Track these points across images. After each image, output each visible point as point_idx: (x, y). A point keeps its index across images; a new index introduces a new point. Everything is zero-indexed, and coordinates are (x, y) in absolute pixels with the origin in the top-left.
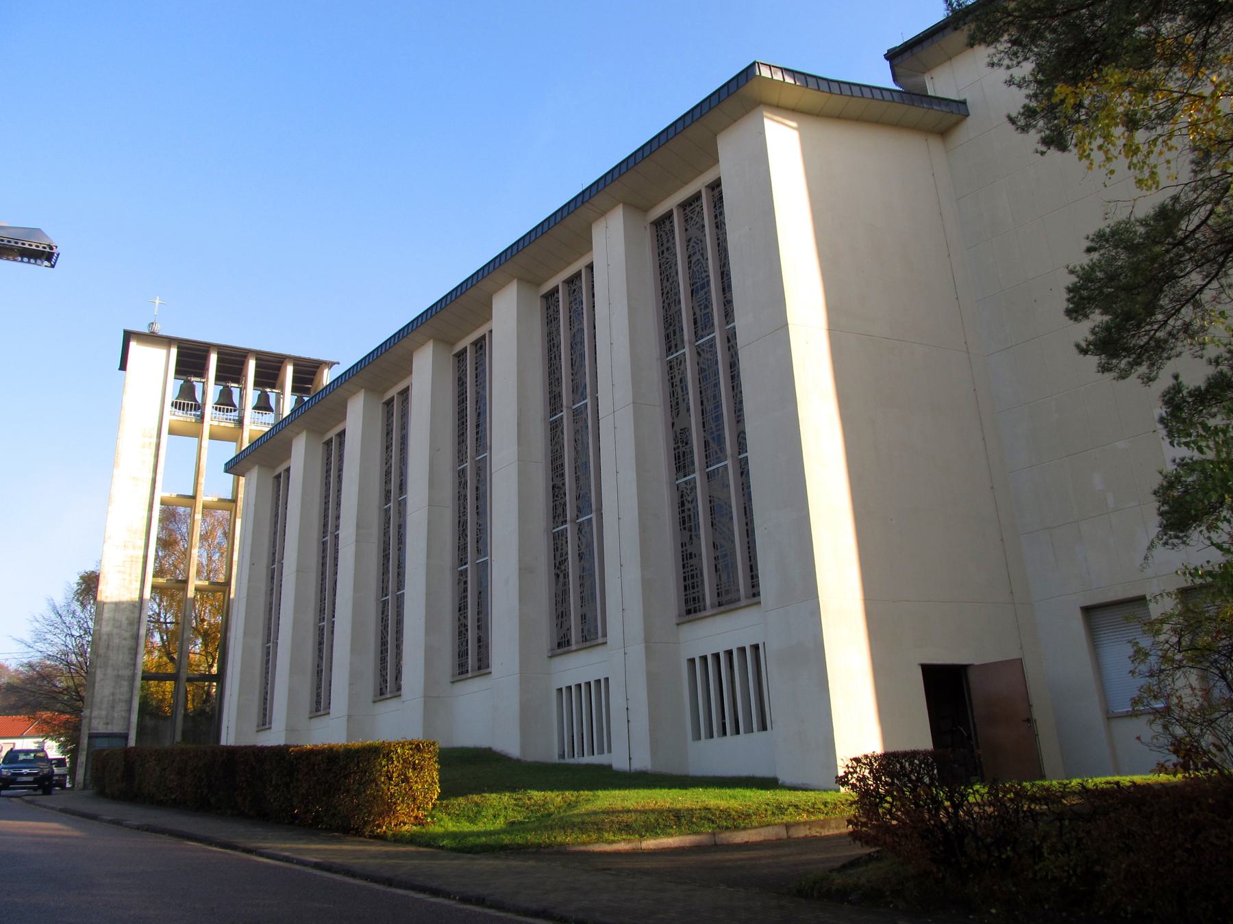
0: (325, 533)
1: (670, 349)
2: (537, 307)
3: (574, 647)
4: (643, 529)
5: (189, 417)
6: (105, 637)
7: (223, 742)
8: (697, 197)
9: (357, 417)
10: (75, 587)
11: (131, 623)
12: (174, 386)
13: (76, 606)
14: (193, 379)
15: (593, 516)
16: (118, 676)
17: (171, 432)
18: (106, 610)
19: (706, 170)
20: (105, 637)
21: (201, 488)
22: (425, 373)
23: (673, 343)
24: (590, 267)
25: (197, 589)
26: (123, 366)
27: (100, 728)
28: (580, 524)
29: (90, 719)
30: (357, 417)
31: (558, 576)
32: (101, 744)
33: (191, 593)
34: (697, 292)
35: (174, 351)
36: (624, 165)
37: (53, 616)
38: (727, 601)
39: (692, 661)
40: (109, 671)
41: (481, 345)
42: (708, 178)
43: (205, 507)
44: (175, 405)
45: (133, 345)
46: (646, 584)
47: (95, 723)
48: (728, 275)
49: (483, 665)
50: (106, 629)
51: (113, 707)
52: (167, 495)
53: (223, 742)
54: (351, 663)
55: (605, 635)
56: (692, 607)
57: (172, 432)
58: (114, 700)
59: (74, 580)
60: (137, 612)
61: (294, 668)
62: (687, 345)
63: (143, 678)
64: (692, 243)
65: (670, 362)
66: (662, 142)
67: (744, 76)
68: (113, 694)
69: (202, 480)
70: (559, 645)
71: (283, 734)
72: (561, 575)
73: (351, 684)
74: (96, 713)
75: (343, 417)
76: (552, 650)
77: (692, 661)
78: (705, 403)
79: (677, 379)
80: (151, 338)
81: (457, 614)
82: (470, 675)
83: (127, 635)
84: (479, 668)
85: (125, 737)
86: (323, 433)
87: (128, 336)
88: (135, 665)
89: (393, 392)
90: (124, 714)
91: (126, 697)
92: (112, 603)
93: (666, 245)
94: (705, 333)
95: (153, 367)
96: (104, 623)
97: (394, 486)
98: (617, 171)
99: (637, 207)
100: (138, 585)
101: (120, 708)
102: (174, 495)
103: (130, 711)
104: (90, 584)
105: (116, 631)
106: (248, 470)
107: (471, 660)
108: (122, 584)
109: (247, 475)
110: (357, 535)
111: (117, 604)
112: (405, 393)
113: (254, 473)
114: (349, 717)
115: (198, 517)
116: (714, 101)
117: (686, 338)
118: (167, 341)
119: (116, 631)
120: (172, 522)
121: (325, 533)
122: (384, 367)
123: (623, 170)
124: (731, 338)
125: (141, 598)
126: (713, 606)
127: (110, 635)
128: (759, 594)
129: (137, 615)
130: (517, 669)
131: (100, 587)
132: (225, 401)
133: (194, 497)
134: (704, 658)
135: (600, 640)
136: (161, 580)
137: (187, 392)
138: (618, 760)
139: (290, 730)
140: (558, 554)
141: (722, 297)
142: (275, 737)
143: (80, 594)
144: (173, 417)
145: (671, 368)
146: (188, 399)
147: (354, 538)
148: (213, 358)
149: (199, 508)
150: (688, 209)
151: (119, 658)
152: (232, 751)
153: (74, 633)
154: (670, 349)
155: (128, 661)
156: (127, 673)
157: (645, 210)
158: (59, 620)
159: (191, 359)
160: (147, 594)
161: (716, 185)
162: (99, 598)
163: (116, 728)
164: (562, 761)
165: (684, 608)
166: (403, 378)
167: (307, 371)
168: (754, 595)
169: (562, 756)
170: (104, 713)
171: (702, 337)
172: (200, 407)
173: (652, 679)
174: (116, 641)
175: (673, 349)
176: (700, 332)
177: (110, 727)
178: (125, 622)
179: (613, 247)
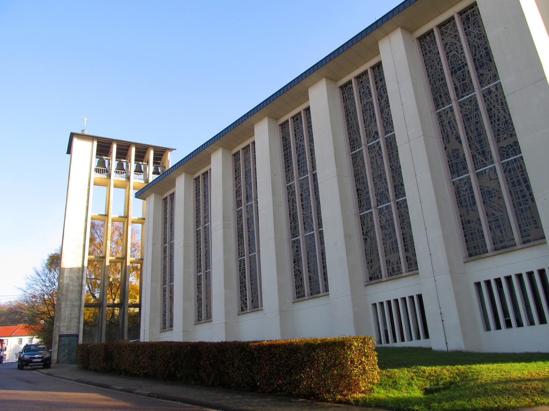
0: (165, 242)
1: (438, 106)
2: (337, 94)
3: (384, 279)
4: (439, 207)
5: (104, 176)
6: (65, 286)
7: (142, 340)
8: (249, 146)
9: (181, 187)
10: (46, 262)
11: (78, 278)
12: (95, 161)
13: (47, 271)
14: (104, 157)
15: (256, 253)
16: (73, 305)
17: (95, 184)
18: (66, 272)
19: (425, 24)
20: (65, 286)
21: (111, 211)
22: (218, 164)
23: (440, 103)
24: (254, 143)
25: (110, 262)
26: (69, 151)
27: (65, 332)
28: (380, 209)
29: (59, 327)
30: (181, 187)
31: (366, 239)
32: (66, 340)
33: (108, 263)
34: (455, 72)
35: (95, 143)
36: (289, 86)
37: (36, 276)
38: (394, 272)
39: (375, 305)
40: (68, 303)
41: (206, 175)
42: (304, 106)
43: (113, 221)
44: (97, 171)
45: (75, 140)
46: (446, 238)
47: (62, 329)
48: (314, 150)
49: (209, 317)
50: (66, 281)
51: (71, 321)
52: (94, 214)
53: (142, 340)
54: (225, 294)
55: (262, 306)
56: (374, 277)
57: (95, 184)
58: (71, 318)
59: (45, 258)
60: (81, 273)
61: (186, 299)
62: (295, 180)
63: (86, 306)
64: (448, 46)
65: (439, 113)
66: (292, 85)
67: (312, 69)
68: (70, 314)
69: (111, 207)
70: (371, 279)
71: (181, 334)
72: (369, 240)
73: (226, 305)
74: (62, 324)
75: (174, 185)
76: (367, 281)
77: (375, 305)
78: (470, 133)
79: (446, 122)
80: (83, 136)
81: (293, 264)
82: (167, 329)
83: (76, 284)
84: (311, 294)
85: (77, 336)
86: (162, 194)
87: (72, 135)
88: (81, 299)
89: (200, 173)
90: (76, 324)
91: (77, 315)
92: (68, 269)
93: (428, 50)
94: (464, 94)
95: (85, 150)
96: (65, 279)
97: (243, 197)
98: (289, 86)
99: (274, 118)
100: (81, 259)
101: (75, 321)
102: (97, 214)
103: (79, 322)
104: (55, 261)
105: (71, 283)
106: (148, 196)
107: (168, 324)
108: (73, 260)
109: (148, 199)
110: (223, 224)
111: (71, 269)
112: (173, 195)
113: (152, 198)
114: (226, 324)
115: (110, 225)
116: (324, 62)
117: (309, 170)
118: (91, 138)
119: (71, 283)
120: (96, 228)
121: (165, 242)
122: (198, 159)
123: (240, 122)
124: (315, 176)
125: (83, 266)
126: (406, 272)
127: (68, 285)
128: (418, 269)
129: (81, 274)
130: (349, 292)
131: (62, 261)
132: (120, 167)
133: (107, 215)
134: (382, 303)
135: (260, 308)
136: (92, 257)
137: (101, 163)
138: (436, 342)
139: (185, 331)
140: (365, 228)
141: (476, 73)
142: (176, 335)
143: (49, 265)
144: (96, 176)
145: (440, 116)
146: (102, 168)
147: (221, 226)
148: (115, 147)
149: (110, 221)
150: (443, 28)
151: (73, 296)
152: (145, 344)
153: (47, 285)
154: (438, 106)
155: (77, 297)
156: (77, 303)
157: (277, 119)
158: (39, 278)
159: (104, 147)
160: (86, 264)
161: (308, 110)
162: (62, 266)
163: (73, 332)
164: (380, 346)
165: (467, 253)
166: (171, 188)
167: (160, 154)
168: (326, 291)
169: (380, 342)
170: (66, 324)
171: (463, 97)
172: (108, 172)
173: (457, 294)
174: (71, 288)
175: (441, 106)
176: (461, 94)
177: (69, 331)
178: (75, 278)
179: (264, 136)
